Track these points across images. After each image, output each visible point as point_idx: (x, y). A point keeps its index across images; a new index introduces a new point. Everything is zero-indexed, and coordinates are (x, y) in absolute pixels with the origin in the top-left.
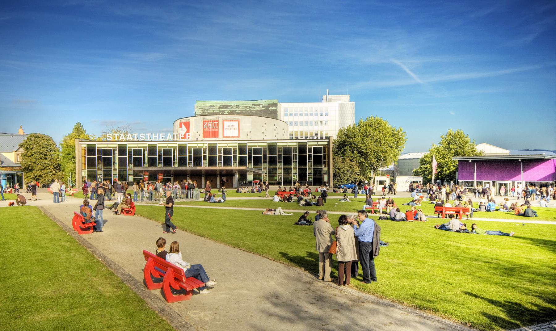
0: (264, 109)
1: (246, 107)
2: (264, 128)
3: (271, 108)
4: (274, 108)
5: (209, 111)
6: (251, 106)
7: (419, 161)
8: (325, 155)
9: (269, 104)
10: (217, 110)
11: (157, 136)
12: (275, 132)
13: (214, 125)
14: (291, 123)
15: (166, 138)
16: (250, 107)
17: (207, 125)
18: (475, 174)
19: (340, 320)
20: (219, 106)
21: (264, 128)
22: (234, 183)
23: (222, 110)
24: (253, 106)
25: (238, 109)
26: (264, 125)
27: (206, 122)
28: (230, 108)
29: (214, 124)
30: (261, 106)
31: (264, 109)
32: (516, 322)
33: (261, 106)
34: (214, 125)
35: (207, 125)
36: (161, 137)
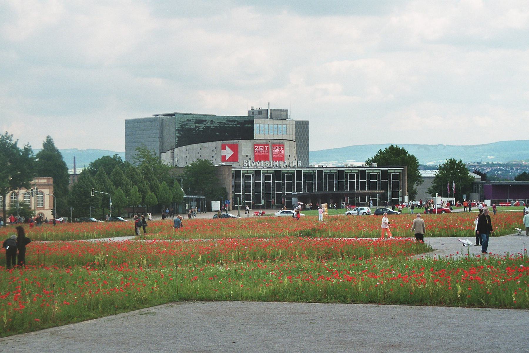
0: (239, 126)
1: (220, 123)
3: (246, 126)
4: (250, 125)
5: (187, 127)
7: (496, 229)
9: (245, 121)
13: (265, 150)
16: (225, 123)
17: (258, 148)
20: (194, 121)
22: (63, 326)
23: (197, 125)
24: (228, 122)
25: (212, 125)
27: (257, 145)
28: (204, 123)
29: (265, 148)
30: (236, 123)
31: (239, 126)
32: (448, 189)
34: (265, 150)
35: (258, 148)
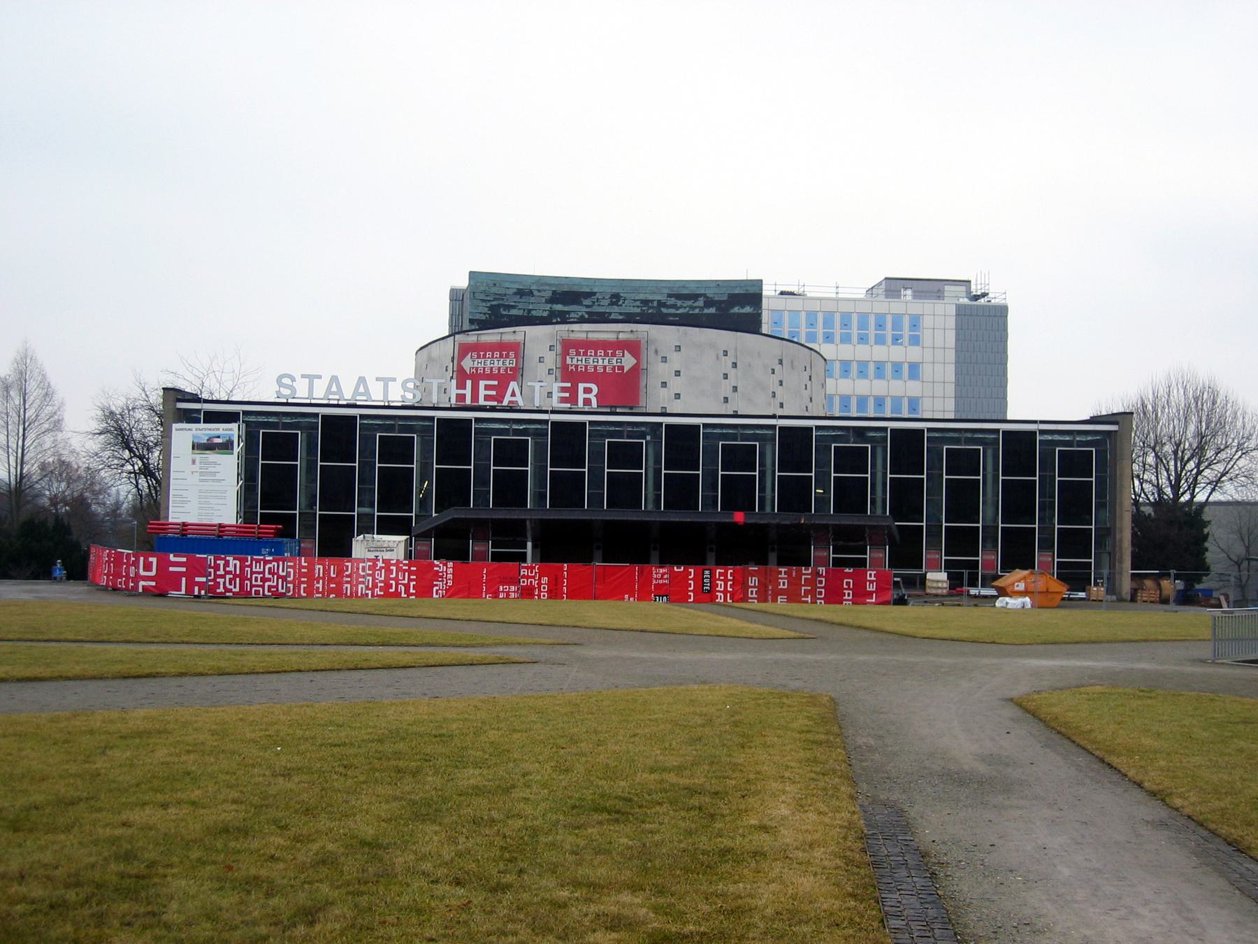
0: (712, 310)
2: (775, 379)
3: (736, 310)
4: (748, 310)
5: (514, 312)
6: (662, 298)
8: (762, 474)
10: (542, 310)
11: (468, 392)
12: (806, 394)
14: (846, 367)
15: (500, 398)
16: (661, 304)
18: (529, 545)
19: (697, 913)
20: (548, 294)
21: (775, 379)
23: (559, 307)
24: (672, 301)
25: (615, 309)
26: (778, 368)
28: (587, 302)
30: (701, 303)
31: (712, 310)
33: (701, 303)
36: (482, 392)
